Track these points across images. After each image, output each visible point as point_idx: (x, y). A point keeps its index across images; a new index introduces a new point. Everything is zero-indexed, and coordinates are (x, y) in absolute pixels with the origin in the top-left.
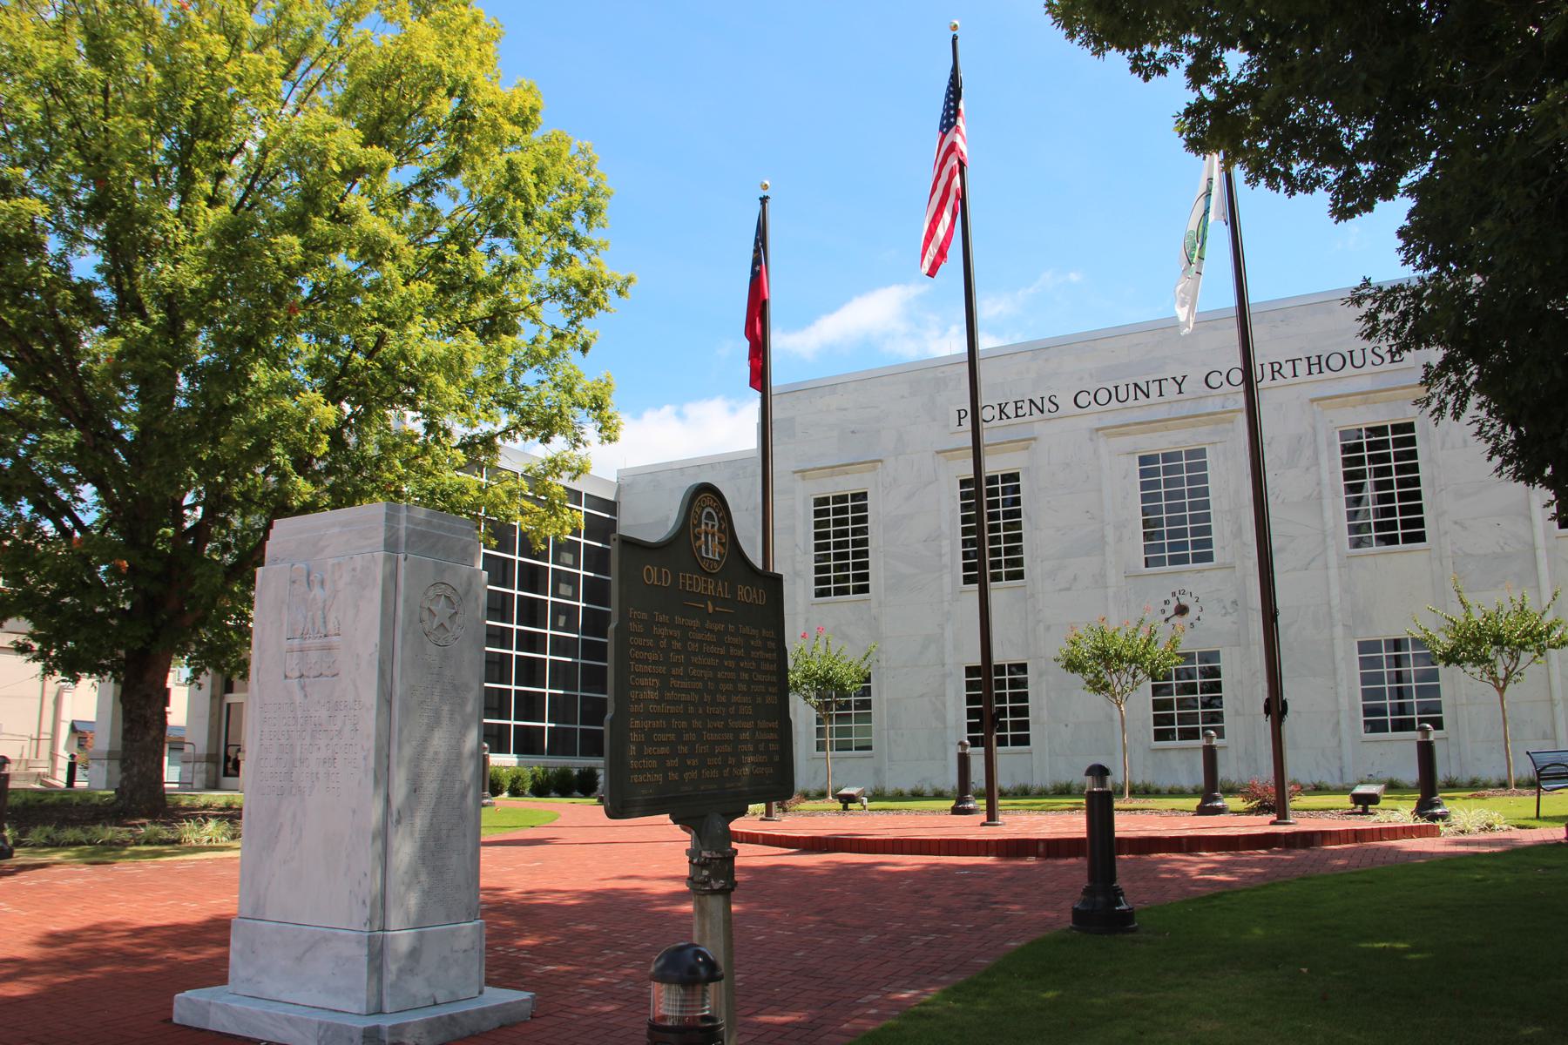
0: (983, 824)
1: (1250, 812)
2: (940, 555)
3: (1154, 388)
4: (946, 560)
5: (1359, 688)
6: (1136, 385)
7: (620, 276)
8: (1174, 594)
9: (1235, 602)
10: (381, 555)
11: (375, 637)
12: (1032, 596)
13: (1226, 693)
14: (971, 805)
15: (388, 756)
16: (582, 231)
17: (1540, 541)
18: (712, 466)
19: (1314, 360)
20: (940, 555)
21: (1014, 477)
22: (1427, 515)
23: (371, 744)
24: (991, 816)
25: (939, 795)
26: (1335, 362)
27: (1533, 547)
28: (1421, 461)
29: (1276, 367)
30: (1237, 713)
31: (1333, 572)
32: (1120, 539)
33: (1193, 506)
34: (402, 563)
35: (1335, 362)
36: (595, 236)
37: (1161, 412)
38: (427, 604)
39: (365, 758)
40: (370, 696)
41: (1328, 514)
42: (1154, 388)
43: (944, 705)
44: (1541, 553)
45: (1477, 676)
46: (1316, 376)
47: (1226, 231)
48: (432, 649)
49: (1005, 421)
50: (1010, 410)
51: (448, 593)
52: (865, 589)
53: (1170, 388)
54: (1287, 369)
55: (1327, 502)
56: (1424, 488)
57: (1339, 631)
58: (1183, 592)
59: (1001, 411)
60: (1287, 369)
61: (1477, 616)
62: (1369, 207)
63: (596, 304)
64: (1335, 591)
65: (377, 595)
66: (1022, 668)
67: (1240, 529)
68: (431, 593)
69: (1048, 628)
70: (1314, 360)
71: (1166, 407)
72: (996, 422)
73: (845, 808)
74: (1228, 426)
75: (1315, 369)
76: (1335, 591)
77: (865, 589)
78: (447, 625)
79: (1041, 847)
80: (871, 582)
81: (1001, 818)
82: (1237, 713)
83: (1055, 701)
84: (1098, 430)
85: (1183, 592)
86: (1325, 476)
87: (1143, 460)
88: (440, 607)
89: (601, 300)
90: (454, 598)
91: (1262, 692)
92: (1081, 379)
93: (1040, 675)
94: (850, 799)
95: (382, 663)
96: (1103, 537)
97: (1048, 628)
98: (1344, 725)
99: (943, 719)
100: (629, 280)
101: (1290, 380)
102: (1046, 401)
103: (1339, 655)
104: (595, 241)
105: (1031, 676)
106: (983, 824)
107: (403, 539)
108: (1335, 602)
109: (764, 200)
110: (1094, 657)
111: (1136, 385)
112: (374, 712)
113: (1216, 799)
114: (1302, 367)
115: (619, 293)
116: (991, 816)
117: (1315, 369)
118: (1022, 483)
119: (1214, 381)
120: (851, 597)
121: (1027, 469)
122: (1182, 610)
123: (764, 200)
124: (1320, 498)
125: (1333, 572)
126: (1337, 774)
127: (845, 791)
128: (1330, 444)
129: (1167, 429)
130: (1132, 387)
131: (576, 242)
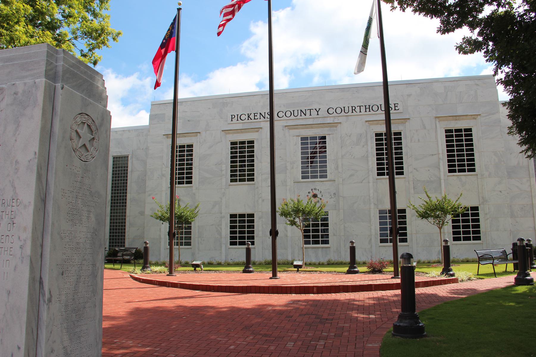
0: (271, 278)
1: (369, 273)
2: (222, 171)
3: (308, 112)
4: (224, 172)
5: (378, 227)
6: (301, 111)
7: (116, 31)
8: (312, 190)
9: (335, 194)
10: (42, 81)
11: (35, 146)
12: (257, 188)
13: (330, 227)
14: (251, 269)
15: (42, 246)
16: (98, 10)
17: (442, 177)
18: (129, 131)
19: (367, 107)
20: (222, 171)
21: (252, 142)
22: (405, 166)
23: (27, 235)
24: (274, 275)
25: (237, 264)
26: (375, 108)
27: (440, 179)
28: (403, 146)
29: (354, 108)
30: (334, 235)
31: (371, 184)
32: (293, 168)
33: (249, 170)
34: (59, 91)
35: (375, 108)
36: (103, 12)
37: (310, 122)
38: (75, 127)
39: (21, 247)
40: (28, 195)
41: (370, 163)
42: (308, 112)
43: (221, 229)
44: (442, 181)
45: (433, 223)
46: (368, 113)
47: (378, 40)
48: (77, 162)
49: (250, 121)
50: (252, 116)
51: (90, 122)
52: (190, 183)
53: (314, 113)
54: (358, 109)
55: (370, 159)
56: (404, 156)
57: (372, 206)
58: (315, 189)
59: (249, 117)
60: (358, 109)
61: (434, 201)
62: (453, 31)
63: (103, 43)
64: (371, 191)
65: (37, 113)
66: (252, 215)
67: (337, 167)
68: (79, 120)
69: (263, 200)
70: (367, 107)
71: (312, 120)
72: (246, 121)
73: (195, 270)
74: (335, 128)
75: (368, 110)
76: (371, 191)
77: (190, 183)
78: (88, 146)
79: (315, 290)
80: (193, 180)
81: (279, 275)
82: (334, 235)
83: (415, 225)
84: (286, 126)
85: (315, 189)
86: (370, 149)
87: (302, 139)
88: (84, 131)
89: (106, 42)
90: (93, 127)
91: (269, 227)
92: (280, 107)
93: (260, 218)
94: (197, 266)
95: (39, 168)
96: (286, 167)
97: (263, 200)
98: (373, 240)
99: (220, 234)
100: (119, 34)
101: (358, 113)
102: (266, 114)
103: (372, 215)
104: (103, 14)
105: (256, 219)
106: (271, 278)
107: (61, 73)
108: (371, 195)
109: (179, 10)
110: (293, 211)
111: (301, 111)
112: (31, 209)
113: (355, 268)
114: (363, 109)
115: (114, 39)
116: (274, 275)
117: (368, 110)
118: (255, 144)
119: (331, 111)
120: (185, 185)
121: (257, 139)
122: (315, 196)
123: (179, 10)
124: (367, 157)
125: (371, 184)
126: (370, 258)
127: (194, 263)
128: (372, 138)
129: (312, 128)
130: (299, 111)
131: (95, 15)
